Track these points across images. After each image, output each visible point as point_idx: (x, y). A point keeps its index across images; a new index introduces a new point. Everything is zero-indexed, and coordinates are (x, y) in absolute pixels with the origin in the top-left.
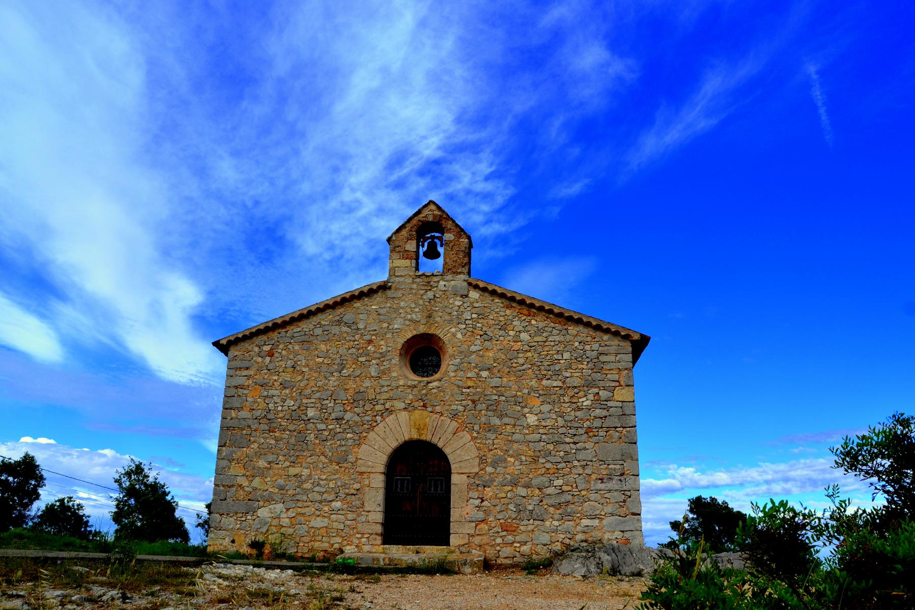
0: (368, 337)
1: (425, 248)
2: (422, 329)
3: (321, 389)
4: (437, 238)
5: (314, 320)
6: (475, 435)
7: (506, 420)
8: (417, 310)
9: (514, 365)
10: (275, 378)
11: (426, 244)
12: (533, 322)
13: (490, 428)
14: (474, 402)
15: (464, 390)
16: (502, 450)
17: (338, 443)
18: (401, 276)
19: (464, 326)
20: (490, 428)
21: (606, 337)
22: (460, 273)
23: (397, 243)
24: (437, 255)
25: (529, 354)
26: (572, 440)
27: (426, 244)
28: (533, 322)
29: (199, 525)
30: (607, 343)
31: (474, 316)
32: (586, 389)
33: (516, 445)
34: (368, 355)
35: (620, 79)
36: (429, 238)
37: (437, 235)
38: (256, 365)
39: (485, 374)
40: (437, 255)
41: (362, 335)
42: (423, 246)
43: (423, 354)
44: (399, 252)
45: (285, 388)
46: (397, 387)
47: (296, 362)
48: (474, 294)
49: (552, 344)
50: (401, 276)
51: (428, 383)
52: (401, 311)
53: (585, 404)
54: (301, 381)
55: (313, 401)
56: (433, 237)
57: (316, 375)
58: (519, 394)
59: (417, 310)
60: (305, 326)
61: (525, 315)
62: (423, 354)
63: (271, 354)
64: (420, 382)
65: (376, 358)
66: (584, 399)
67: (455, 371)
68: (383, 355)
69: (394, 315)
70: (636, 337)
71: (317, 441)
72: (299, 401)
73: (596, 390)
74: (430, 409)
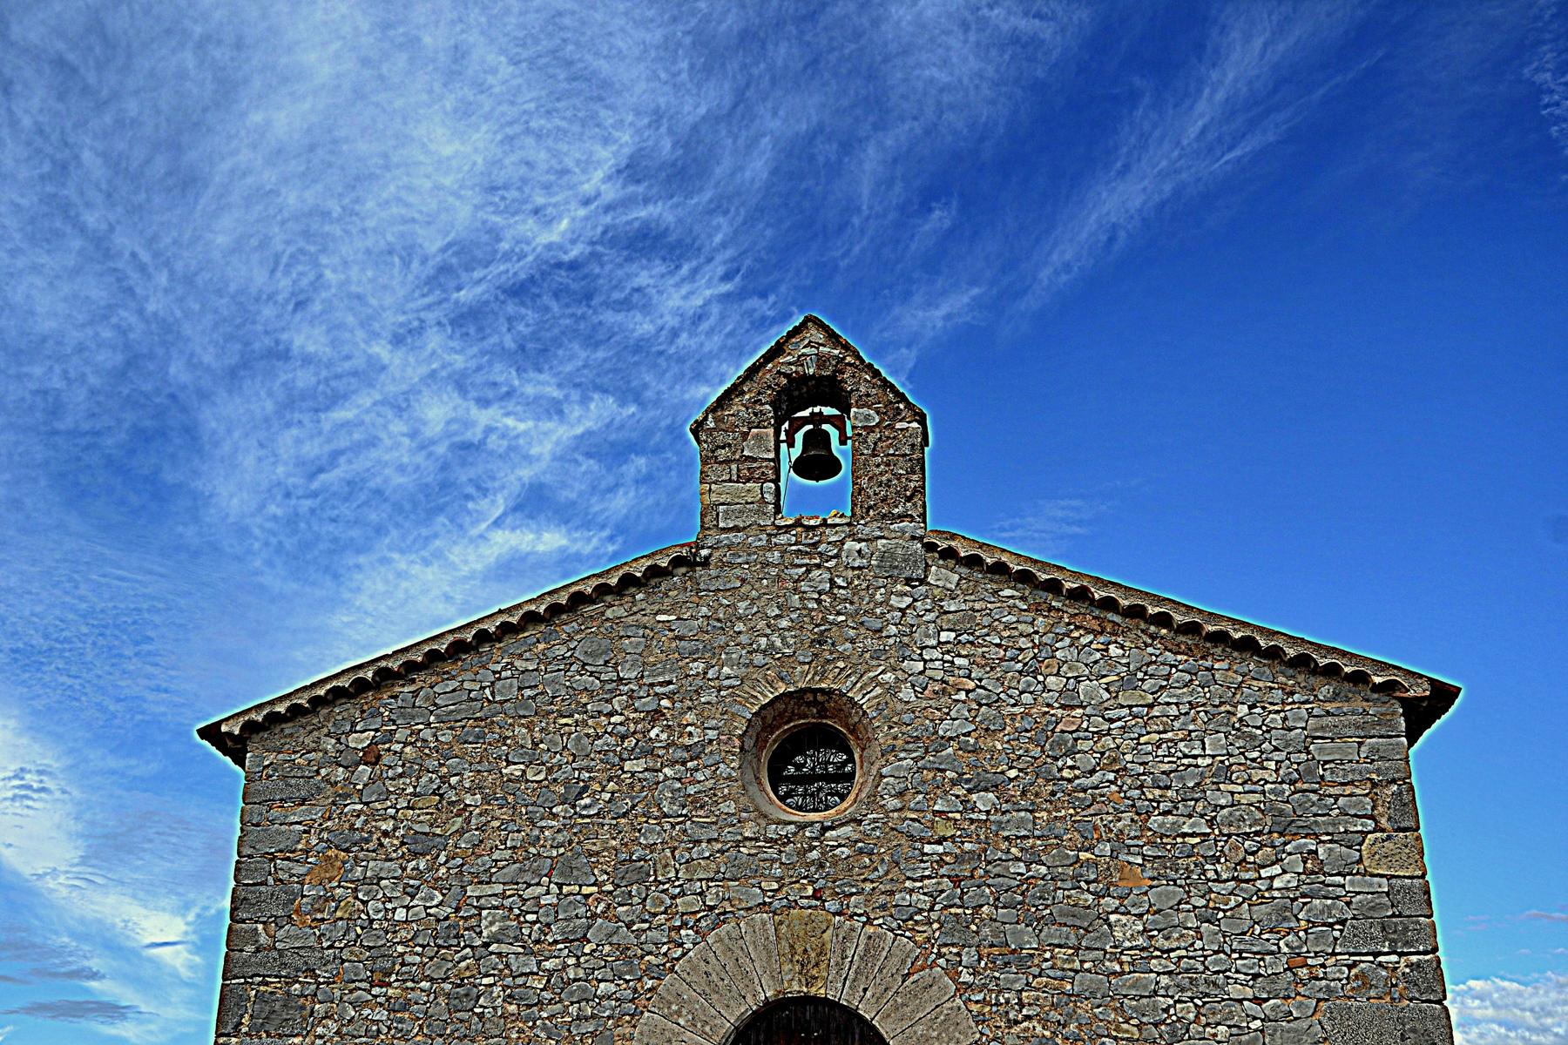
0: (648, 703)
1: (797, 451)
2: (802, 679)
3: (521, 854)
4: (828, 419)
5: (497, 659)
6: (966, 977)
7: (1052, 933)
8: (784, 623)
9: (1066, 773)
10: (387, 826)
11: (799, 437)
12: (1114, 650)
13: (1016, 959)
14: (956, 880)
15: (927, 848)
16: (1045, 1023)
17: (573, 1010)
18: (736, 529)
19: (920, 666)
20: (1016, 959)
21: (1325, 691)
22: (901, 517)
23: (720, 438)
24: (832, 467)
25: (1108, 742)
26: (1249, 993)
27: (799, 437)
28: (1114, 650)
29: (183, 191)
30: (1330, 707)
31: (944, 636)
32: (1279, 841)
33: (1087, 1005)
34: (652, 752)
35: (114, 925)
36: (805, 421)
37: (828, 411)
38: (330, 791)
39: (984, 800)
40: (832, 467)
41: (631, 695)
42: (791, 444)
43: (805, 741)
44: (728, 462)
45: (416, 855)
46: (737, 845)
47: (444, 779)
48: (942, 576)
49: (1173, 711)
50: (736, 529)
51: (825, 829)
52: (740, 627)
53: (1277, 884)
54: (461, 832)
55: (498, 889)
56: (818, 419)
57: (505, 814)
58: (1084, 855)
59: (784, 623)
60: (466, 678)
61: (1089, 631)
62: (805, 741)
63: (371, 756)
64: (802, 826)
65: (673, 763)
66: (1277, 869)
67: (900, 794)
68: (695, 751)
69: (722, 639)
70: (1420, 691)
71: (512, 1008)
72: (456, 890)
73: (1311, 844)
74: (832, 905)
